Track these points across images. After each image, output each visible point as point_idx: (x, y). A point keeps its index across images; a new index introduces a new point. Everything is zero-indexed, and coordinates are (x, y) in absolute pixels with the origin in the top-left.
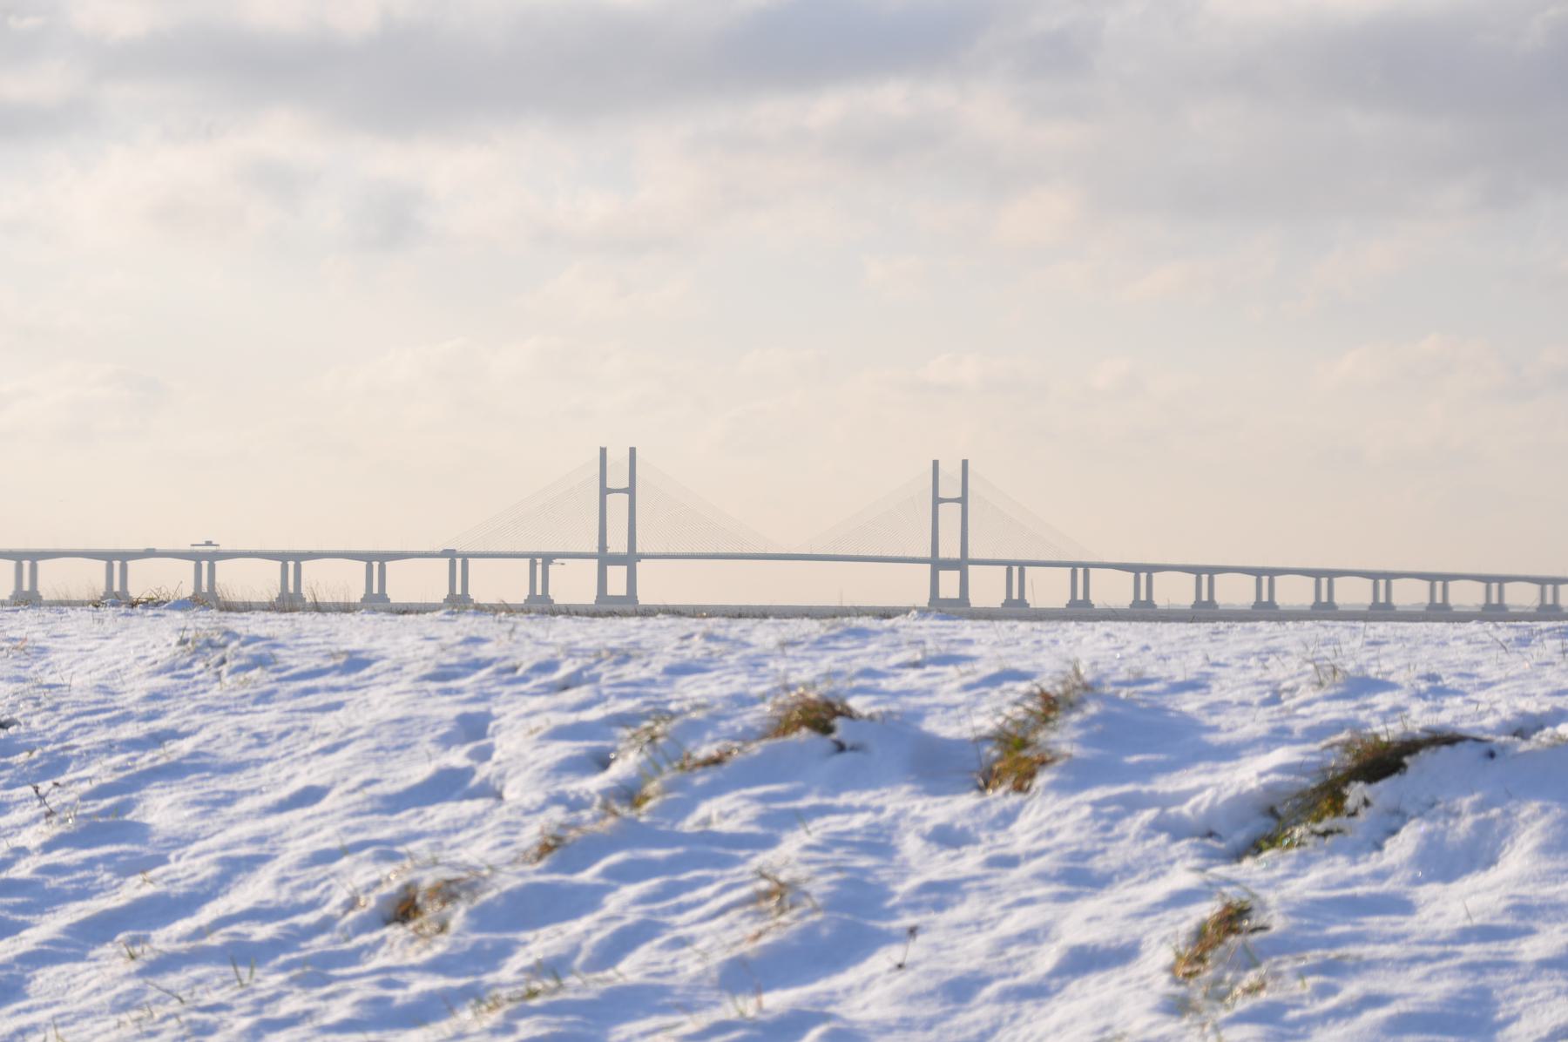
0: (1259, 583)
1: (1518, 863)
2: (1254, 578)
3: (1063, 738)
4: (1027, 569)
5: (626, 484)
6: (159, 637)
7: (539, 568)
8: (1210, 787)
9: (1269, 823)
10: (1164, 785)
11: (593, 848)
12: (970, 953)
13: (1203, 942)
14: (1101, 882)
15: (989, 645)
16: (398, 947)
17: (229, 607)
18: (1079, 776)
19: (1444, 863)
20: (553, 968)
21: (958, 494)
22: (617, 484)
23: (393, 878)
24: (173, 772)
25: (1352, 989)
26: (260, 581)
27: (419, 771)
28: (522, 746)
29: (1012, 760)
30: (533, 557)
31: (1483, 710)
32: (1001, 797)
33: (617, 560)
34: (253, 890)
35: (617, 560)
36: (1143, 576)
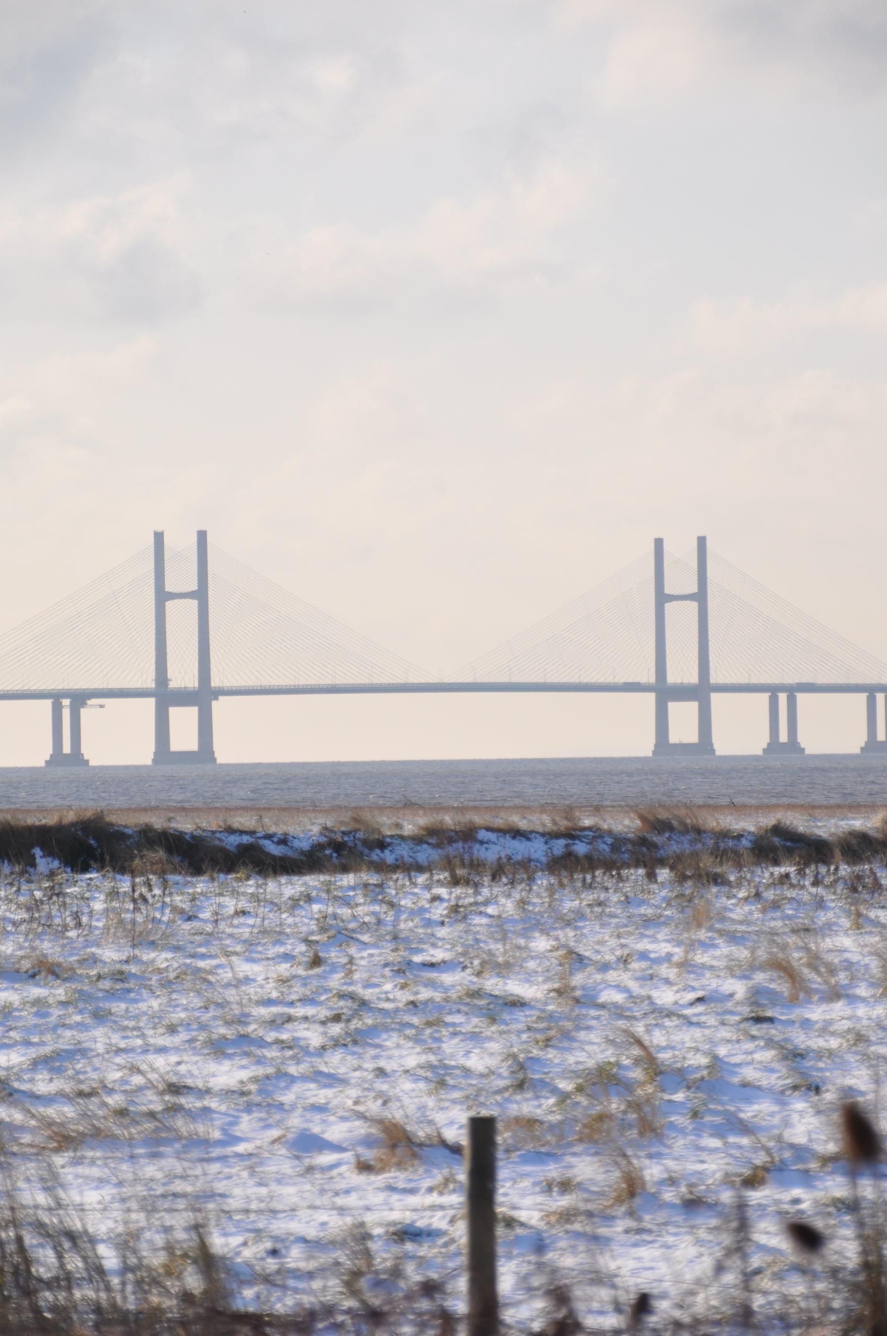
5: (694, 588)
7: (66, 714)
22: (182, 583)
30: (56, 697)
33: (184, 698)
35: (184, 698)
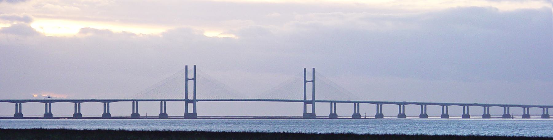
0: (524, 109)
2: (420, 106)
4: (167, 102)
21: (193, 77)
33: (191, 101)
36: (507, 108)
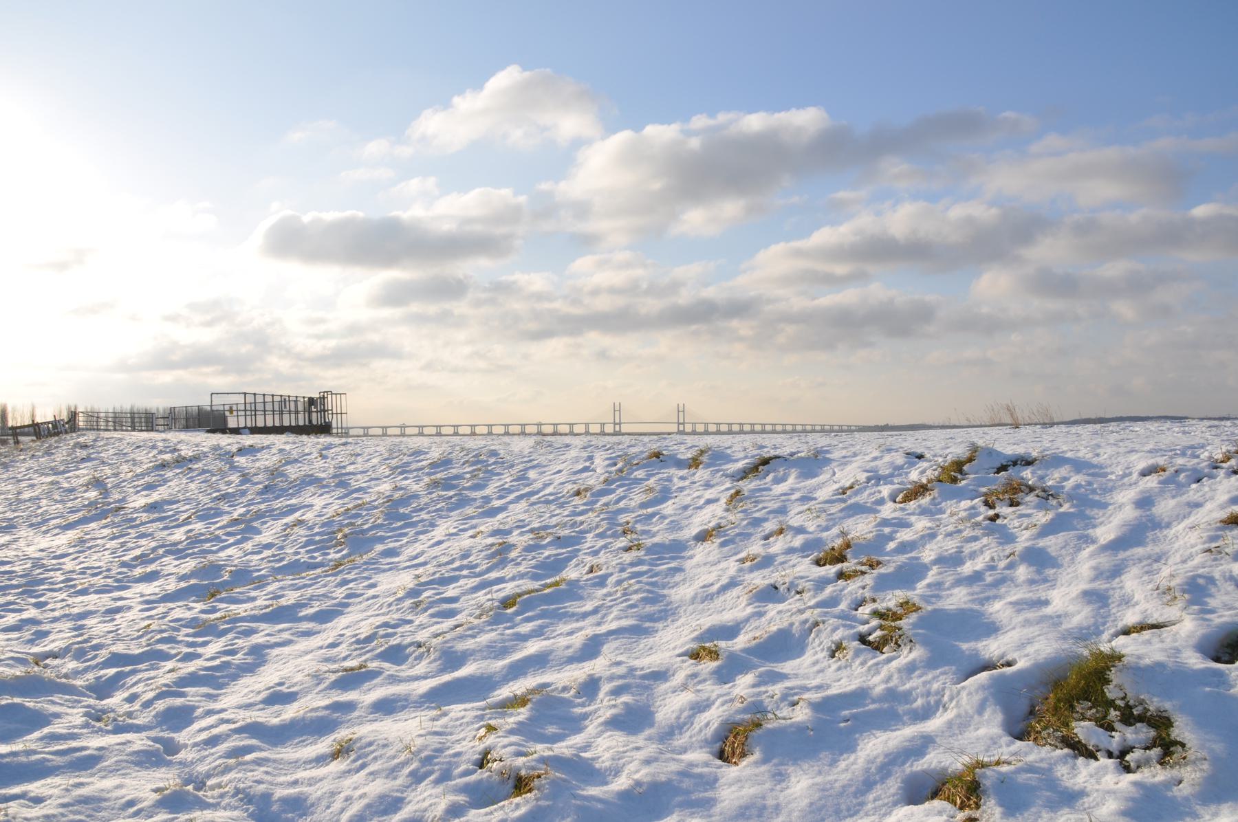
1: (791, 480)
3: (705, 458)
6: (531, 441)
8: (733, 467)
9: (744, 474)
10: (724, 467)
11: (614, 481)
12: (687, 500)
13: (732, 497)
14: (712, 486)
15: (690, 440)
16: (577, 501)
17: (544, 435)
18: (708, 466)
19: (778, 481)
20: (607, 504)
23: (576, 487)
24: (534, 467)
25: (760, 506)
26: (501, 430)
27: (581, 467)
28: (600, 462)
29: (695, 463)
31: (784, 451)
32: (693, 470)
34: (549, 490)
